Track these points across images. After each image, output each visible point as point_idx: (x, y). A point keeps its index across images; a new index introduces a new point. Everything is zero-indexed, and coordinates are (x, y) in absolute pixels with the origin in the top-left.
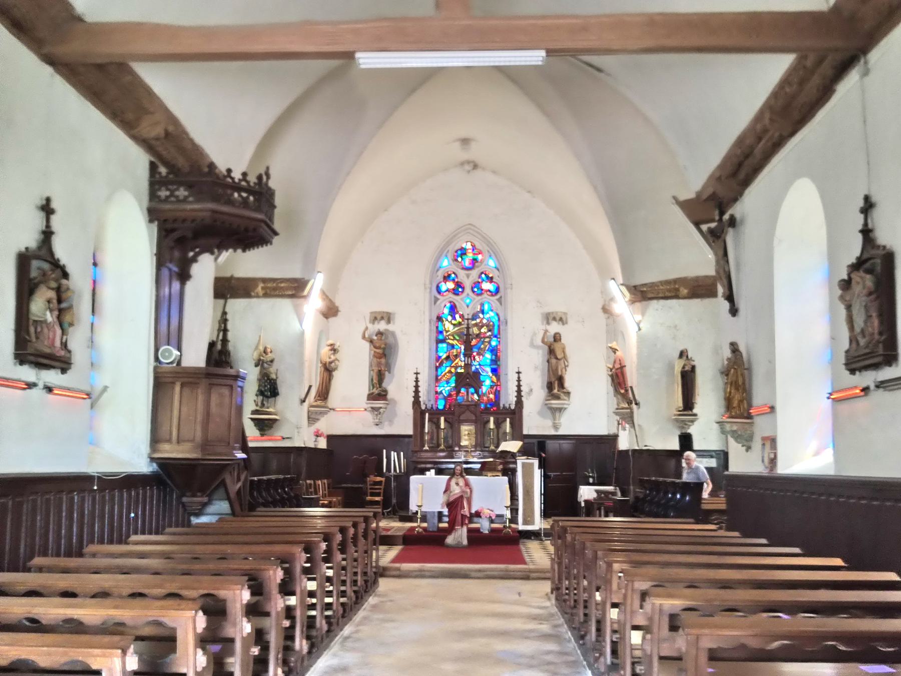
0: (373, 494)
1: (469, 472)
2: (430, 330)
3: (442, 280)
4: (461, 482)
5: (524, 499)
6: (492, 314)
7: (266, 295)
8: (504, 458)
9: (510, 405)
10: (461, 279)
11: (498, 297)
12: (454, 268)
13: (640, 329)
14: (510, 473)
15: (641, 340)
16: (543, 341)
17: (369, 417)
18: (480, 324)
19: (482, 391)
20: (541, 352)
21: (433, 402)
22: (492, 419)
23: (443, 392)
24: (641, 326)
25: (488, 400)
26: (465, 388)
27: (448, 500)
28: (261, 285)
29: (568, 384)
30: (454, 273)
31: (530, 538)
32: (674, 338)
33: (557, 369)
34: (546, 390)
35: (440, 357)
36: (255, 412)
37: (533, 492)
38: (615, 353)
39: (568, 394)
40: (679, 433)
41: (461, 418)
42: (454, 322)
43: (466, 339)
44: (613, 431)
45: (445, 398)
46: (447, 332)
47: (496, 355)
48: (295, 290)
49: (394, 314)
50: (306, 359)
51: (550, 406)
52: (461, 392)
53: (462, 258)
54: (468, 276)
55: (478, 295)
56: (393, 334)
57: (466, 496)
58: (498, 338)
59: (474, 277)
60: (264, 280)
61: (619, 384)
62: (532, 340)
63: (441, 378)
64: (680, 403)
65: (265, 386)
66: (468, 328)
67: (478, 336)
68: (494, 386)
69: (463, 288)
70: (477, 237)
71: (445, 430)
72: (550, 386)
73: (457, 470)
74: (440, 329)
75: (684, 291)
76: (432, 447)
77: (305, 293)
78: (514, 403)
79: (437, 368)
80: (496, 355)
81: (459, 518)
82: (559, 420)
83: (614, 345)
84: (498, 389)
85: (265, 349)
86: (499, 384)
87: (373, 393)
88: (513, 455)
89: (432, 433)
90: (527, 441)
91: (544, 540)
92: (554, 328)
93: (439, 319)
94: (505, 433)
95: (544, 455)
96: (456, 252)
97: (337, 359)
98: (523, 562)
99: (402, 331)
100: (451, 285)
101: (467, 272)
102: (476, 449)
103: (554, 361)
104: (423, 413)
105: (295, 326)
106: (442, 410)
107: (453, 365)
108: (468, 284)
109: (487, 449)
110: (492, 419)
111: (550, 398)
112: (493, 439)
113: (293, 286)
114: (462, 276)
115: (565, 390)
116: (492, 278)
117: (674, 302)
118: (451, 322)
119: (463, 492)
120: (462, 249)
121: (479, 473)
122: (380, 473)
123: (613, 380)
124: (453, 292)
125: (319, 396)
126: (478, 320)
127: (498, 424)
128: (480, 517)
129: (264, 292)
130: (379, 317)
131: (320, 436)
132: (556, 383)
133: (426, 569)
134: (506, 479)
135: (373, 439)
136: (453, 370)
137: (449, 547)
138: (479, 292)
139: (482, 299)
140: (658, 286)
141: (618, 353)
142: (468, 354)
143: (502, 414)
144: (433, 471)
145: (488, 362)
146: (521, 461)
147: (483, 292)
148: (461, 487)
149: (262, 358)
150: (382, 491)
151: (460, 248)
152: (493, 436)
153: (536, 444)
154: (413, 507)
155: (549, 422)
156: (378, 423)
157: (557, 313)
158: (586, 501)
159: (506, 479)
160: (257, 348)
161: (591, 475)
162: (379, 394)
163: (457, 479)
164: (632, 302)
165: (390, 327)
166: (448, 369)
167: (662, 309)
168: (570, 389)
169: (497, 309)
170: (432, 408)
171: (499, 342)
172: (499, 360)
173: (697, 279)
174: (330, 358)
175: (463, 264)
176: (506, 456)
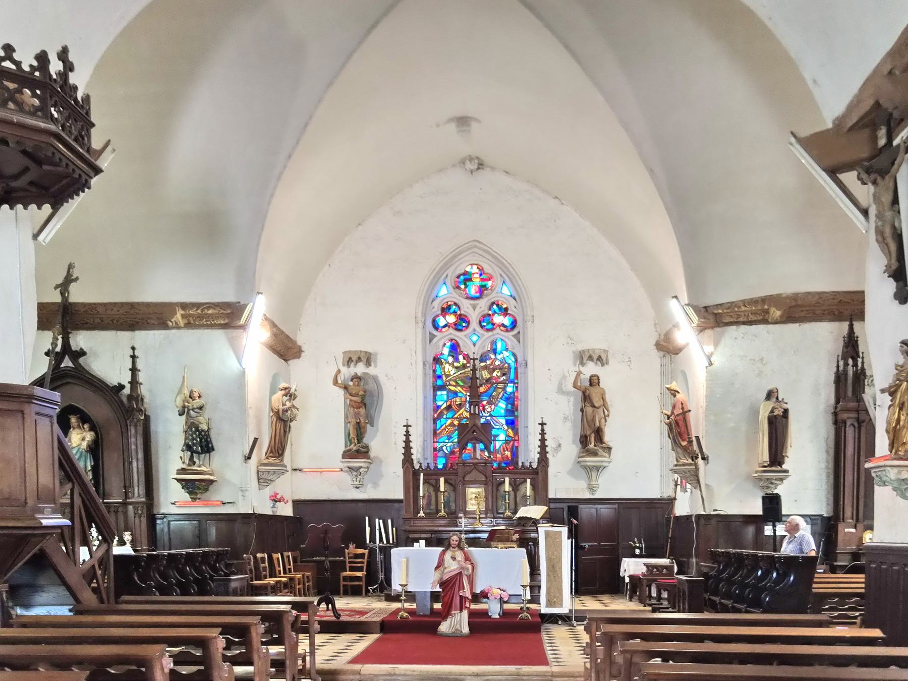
0: (352, 569)
1: (474, 543)
2: (425, 374)
3: (440, 312)
4: (459, 555)
5: (548, 575)
6: (506, 354)
7: (188, 325)
8: (524, 526)
9: (530, 463)
10: (465, 311)
11: (515, 332)
12: (456, 297)
13: (711, 364)
14: (528, 543)
15: (713, 379)
16: (575, 386)
17: (347, 478)
18: (491, 367)
19: (495, 447)
20: (572, 399)
21: (430, 460)
22: (507, 480)
23: (444, 448)
24: (712, 359)
25: (503, 458)
26: (471, 443)
27: (441, 579)
28: (180, 312)
29: (608, 438)
30: (455, 304)
31: (557, 623)
32: (760, 374)
33: (593, 419)
34: (580, 446)
35: (439, 407)
36: (182, 471)
37: (561, 568)
38: (675, 396)
39: (609, 449)
40: (762, 494)
41: (467, 479)
42: (455, 364)
43: (472, 384)
44: (668, 493)
45: (446, 456)
46: (447, 376)
47: (513, 404)
48: (228, 317)
49: (376, 354)
50: (249, 406)
51: (583, 464)
52: (468, 448)
53: (465, 284)
54: (474, 308)
55: (488, 330)
56: (375, 379)
57: (466, 573)
58: (514, 383)
59: (483, 309)
60: (184, 306)
61: (680, 434)
62: (560, 384)
63: (440, 433)
64: (766, 457)
65: (193, 439)
66: (474, 370)
67: (488, 380)
68: (510, 441)
69: (468, 323)
70: (486, 258)
71: (446, 494)
72: (584, 441)
73: (453, 541)
74: (438, 373)
75: (776, 313)
76: (429, 513)
77: (242, 322)
78: (537, 461)
79: (435, 421)
80: (513, 404)
81: (457, 600)
82: (596, 480)
83: (674, 386)
84: (516, 444)
85: (191, 392)
86: (516, 438)
87: (350, 450)
88: (535, 522)
89: (430, 497)
90: (552, 505)
91: (575, 625)
92: (590, 369)
93: (437, 360)
94: (525, 496)
95: (575, 522)
96: (458, 277)
97: (293, 406)
98: (544, 662)
99: (386, 376)
100: (451, 319)
101: (472, 302)
102: (486, 515)
103: (589, 410)
104: (416, 474)
105: (232, 364)
106: (442, 469)
107: (456, 416)
108: (474, 317)
109: (502, 516)
110: (507, 480)
111: (584, 454)
112: (509, 503)
113: (225, 312)
114: (466, 307)
115: (604, 445)
116: (506, 309)
117: (761, 328)
118: (452, 364)
119: (463, 568)
120: (466, 273)
121: (487, 543)
122: (361, 544)
123: (671, 429)
124: (454, 327)
125: (271, 452)
126: (488, 362)
127: (515, 486)
128: (488, 598)
129: (186, 321)
130: (354, 359)
131: (280, 501)
132: (593, 436)
133: (397, 673)
134: (524, 550)
135: (353, 505)
136: (456, 422)
137: (446, 636)
138: (490, 326)
139: (493, 335)
140: (739, 307)
141: (678, 396)
142: (475, 399)
143: (520, 473)
144: (422, 542)
145: (503, 412)
146: (543, 530)
147: (495, 327)
148: (459, 562)
149: (187, 404)
150: (365, 565)
151: (463, 271)
152: (509, 500)
153: (566, 509)
154: (396, 587)
155: (583, 484)
156: (358, 486)
157: (594, 350)
158: (631, 577)
159: (524, 550)
160: (180, 392)
161: (639, 546)
162: (358, 451)
163: (454, 552)
164: (701, 329)
165: (372, 371)
166: (449, 421)
167: (743, 338)
168: (611, 444)
169: (513, 348)
170: (428, 467)
171: (517, 387)
172: (517, 410)
173: (795, 297)
174: (283, 405)
175: (468, 292)
176: (526, 523)
